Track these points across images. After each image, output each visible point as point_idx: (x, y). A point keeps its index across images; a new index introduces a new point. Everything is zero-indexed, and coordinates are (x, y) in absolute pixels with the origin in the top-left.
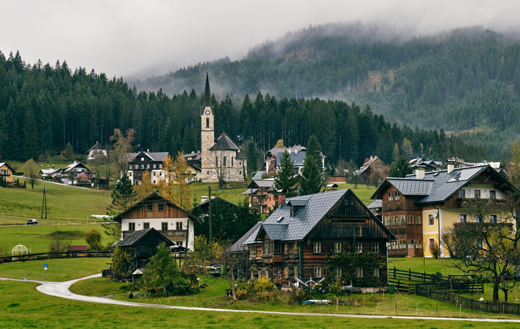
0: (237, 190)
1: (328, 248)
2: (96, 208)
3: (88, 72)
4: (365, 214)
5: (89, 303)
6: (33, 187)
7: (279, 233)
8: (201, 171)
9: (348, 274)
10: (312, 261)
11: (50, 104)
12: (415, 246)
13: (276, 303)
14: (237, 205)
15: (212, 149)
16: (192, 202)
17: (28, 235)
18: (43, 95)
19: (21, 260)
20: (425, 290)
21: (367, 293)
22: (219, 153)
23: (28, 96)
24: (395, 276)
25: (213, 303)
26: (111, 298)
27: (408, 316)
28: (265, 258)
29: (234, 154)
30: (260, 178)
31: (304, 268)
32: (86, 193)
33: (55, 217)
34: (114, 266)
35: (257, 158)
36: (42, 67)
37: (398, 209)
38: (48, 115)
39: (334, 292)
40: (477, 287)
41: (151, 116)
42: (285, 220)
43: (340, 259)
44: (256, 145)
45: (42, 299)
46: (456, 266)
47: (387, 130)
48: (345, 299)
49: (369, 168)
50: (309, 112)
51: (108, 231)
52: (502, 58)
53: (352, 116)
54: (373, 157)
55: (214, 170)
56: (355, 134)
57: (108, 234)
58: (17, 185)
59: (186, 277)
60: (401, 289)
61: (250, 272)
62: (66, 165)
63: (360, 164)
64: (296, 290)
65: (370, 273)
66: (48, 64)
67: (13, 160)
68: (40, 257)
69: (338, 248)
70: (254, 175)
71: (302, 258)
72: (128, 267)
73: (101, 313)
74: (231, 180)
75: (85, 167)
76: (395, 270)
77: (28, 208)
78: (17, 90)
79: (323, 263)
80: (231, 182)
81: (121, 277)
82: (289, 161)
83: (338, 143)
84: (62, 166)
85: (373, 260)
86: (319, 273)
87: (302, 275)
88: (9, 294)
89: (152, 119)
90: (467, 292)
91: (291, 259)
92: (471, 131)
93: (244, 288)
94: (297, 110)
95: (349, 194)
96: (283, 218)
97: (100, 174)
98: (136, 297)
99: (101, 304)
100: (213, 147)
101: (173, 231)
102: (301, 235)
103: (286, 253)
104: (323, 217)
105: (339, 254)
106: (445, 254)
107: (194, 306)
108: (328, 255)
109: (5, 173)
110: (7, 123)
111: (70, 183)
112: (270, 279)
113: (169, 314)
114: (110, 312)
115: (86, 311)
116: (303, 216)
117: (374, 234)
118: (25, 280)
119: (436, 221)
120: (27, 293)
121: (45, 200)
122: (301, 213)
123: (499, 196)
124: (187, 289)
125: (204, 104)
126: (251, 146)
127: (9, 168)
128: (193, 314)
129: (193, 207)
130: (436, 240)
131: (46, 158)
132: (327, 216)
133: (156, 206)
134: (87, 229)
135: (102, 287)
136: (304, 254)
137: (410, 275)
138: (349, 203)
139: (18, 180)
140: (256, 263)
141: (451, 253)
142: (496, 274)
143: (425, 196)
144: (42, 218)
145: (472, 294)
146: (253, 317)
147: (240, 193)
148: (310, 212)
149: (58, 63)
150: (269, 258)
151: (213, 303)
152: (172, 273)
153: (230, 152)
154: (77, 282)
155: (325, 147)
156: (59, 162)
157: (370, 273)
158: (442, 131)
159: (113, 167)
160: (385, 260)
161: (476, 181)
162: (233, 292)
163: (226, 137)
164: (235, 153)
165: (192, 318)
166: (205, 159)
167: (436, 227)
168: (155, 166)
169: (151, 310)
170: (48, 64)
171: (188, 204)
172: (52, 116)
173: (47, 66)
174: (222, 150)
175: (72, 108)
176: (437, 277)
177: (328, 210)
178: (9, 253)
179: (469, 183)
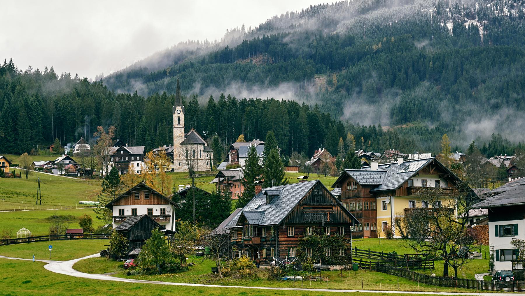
0: (205, 179)
1: (300, 232)
2: (83, 195)
3: (73, 77)
4: (332, 202)
5: (93, 280)
6: (27, 177)
7: (257, 218)
8: (173, 162)
9: (318, 254)
10: (287, 243)
11: (40, 104)
12: (370, 229)
13: (256, 279)
14: (211, 193)
15: (182, 144)
16: (171, 190)
17: (28, 219)
18: (34, 97)
19: (26, 242)
20: (384, 267)
21: (334, 270)
22: (189, 147)
23: (21, 98)
24: (356, 255)
25: (202, 279)
26: (111, 275)
27: (373, 290)
28: (246, 240)
29: (201, 148)
30: (225, 168)
31: (280, 249)
32: (74, 181)
33: (48, 203)
34: (112, 247)
35: (221, 151)
36: (32, 73)
37: (356, 197)
38: (38, 114)
39: (306, 269)
40: (429, 264)
41: (128, 115)
42: (261, 208)
43: (311, 241)
44: (220, 139)
45: (51, 277)
46: (412, 247)
47: (333, 126)
48: (317, 275)
49: (319, 159)
50: (265, 111)
51: (99, 216)
52: (431, 62)
53: (302, 114)
54: (322, 150)
55: (185, 162)
56: (306, 131)
57: (99, 218)
58: (14, 175)
59: (176, 256)
60: (365, 267)
61: (231, 252)
62: (55, 157)
63: (310, 156)
64: (273, 268)
65: (336, 253)
66: (38, 70)
67: (8, 153)
68: (41, 239)
69: (309, 232)
70: (219, 165)
71: (278, 240)
72: (124, 248)
73: (105, 289)
74: (199, 170)
75: (72, 160)
76: (356, 249)
77: (24, 195)
78: (11, 93)
79: (296, 244)
80: (200, 172)
81: (116, 254)
82: (256, 154)
83: (291, 138)
84: (52, 159)
85: (339, 242)
86: (292, 254)
87: (278, 255)
88: (21, 272)
89: (129, 117)
90: (420, 268)
91: (268, 241)
92: (404, 126)
93: (228, 267)
94: (255, 109)
95: (319, 185)
96: (260, 206)
97: (86, 165)
98: (134, 274)
99: (103, 281)
100: (183, 142)
101: (158, 216)
102: (277, 220)
103: (263, 236)
104: (296, 205)
105: (310, 236)
106: (397, 235)
107: (185, 282)
108: (300, 237)
109: (3, 165)
110: (3, 121)
111: (59, 173)
112: (249, 258)
113: (165, 289)
114: (112, 287)
115: (91, 287)
116: (278, 203)
117: (340, 219)
118: (33, 260)
119: (388, 207)
120: (37, 271)
121: (39, 189)
122: (276, 201)
123: (442, 184)
124: (178, 268)
125: (175, 104)
126: (216, 140)
127: (7, 160)
128: (186, 289)
129: (172, 195)
130: (389, 222)
131: (37, 151)
132: (299, 204)
133: (142, 195)
134: (80, 213)
135: (102, 266)
136: (280, 236)
137: (369, 254)
138: (318, 193)
139: (14, 171)
140: (237, 245)
141: (402, 233)
142: (446, 252)
143: (379, 185)
144: (37, 204)
145: (424, 270)
146: (238, 292)
147: (207, 181)
148: (284, 200)
149: (46, 68)
150: (249, 240)
151: (202, 279)
152: (164, 254)
153: (199, 145)
154: (79, 261)
155: (280, 140)
156: (49, 155)
157: (336, 253)
158: (380, 126)
159: (96, 159)
160: (349, 242)
161: (424, 171)
162: (219, 270)
163: (195, 132)
164: (203, 146)
165: (185, 293)
166: (177, 152)
167: (392, 212)
168: (133, 158)
169: (149, 286)
170: (38, 70)
171: (168, 192)
172: (42, 115)
173: (37, 72)
174: (192, 144)
175: (60, 108)
176: (392, 257)
177: (300, 198)
178: (14, 235)
179: (417, 174)
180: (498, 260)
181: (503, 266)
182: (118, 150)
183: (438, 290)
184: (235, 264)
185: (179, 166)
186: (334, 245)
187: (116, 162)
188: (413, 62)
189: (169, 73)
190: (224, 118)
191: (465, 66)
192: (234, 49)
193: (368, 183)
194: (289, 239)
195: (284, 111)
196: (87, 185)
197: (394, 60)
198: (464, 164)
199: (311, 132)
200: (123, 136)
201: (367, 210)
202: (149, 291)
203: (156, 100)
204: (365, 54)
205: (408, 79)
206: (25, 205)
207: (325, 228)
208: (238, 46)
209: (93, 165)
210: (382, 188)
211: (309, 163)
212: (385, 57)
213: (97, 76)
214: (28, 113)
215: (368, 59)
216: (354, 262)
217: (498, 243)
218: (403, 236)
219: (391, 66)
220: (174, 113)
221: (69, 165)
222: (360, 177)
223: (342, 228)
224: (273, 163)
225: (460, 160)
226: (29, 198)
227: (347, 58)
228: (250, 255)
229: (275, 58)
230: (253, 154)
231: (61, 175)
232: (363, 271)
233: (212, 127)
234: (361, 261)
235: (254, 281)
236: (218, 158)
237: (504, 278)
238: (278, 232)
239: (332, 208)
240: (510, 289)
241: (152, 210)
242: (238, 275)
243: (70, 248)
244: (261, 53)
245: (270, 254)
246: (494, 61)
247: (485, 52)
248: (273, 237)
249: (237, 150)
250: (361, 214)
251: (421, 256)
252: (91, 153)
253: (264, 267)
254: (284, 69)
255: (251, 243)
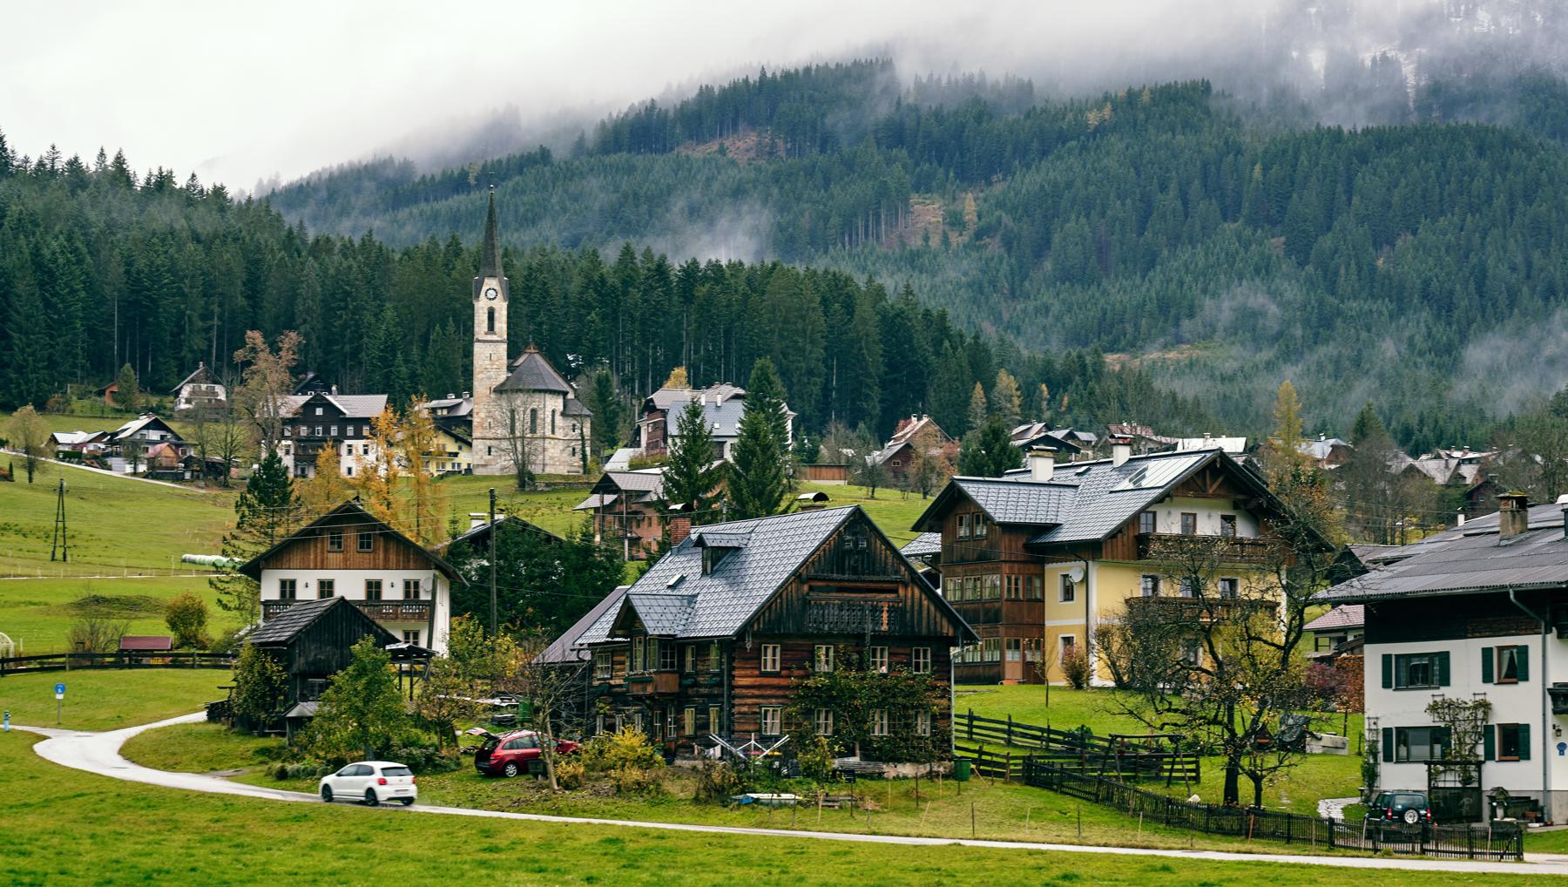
0: (564, 496)
1: (799, 656)
2: (195, 535)
4: (897, 572)
5: (172, 790)
6: (30, 480)
8: (470, 445)
10: (757, 692)
11: (80, 262)
12: (1024, 656)
15: (500, 390)
16: (446, 526)
17: (17, 604)
20: (1048, 771)
21: (897, 778)
22: (519, 400)
23: (22, 241)
24: (970, 733)
26: (229, 778)
30: (626, 467)
32: (171, 495)
33: (88, 559)
35: (616, 414)
36: (58, 166)
38: (73, 292)
39: (812, 773)
40: (1184, 766)
41: (344, 300)
42: (687, 585)
43: (831, 688)
44: (615, 380)
45: (48, 778)
47: (955, 349)
48: (841, 792)
49: (908, 446)
50: (755, 297)
51: (225, 599)
52: (1258, 167)
53: (864, 309)
54: (919, 419)
56: (875, 359)
57: (225, 607)
59: (427, 726)
60: (991, 770)
61: (594, 717)
63: (884, 433)
66: (76, 159)
68: (45, 664)
70: (609, 457)
72: (274, 698)
73: (202, 819)
74: (548, 470)
77: (17, 532)
79: (785, 697)
80: (549, 475)
83: (828, 381)
84: (108, 426)
86: (773, 725)
89: (345, 308)
90: (1158, 778)
91: (701, 686)
95: (858, 520)
96: (682, 579)
97: (208, 448)
98: (296, 775)
99: (202, 794)
103: (689, 669)
106: (1101, 676)
107: (446, 804)
111: (129, 469)
112: (644, 737)
114: (224, 815)
116: (734, 573)
117: (920, 623)
119: (1079, 593)
120: (10, 760)
121: (61, 516)
123: (1244, 530)
126: (603, 383)
129: (448, 542)
131: (68, 402)
132: (797, 576)
133: (351, 537)
134: (171, 590)
135: (206, 749)
137: (1010, 732)
138: (856, 544)
140: (610, 694)
143: (1055, 527)
146: (599, 838)
147: (571, 504)
150: (644, 681)
152: (388, 717)
153: (548, 396)
155: (796, 388)
160: (946, 693)
163: (538, 357)
166: (482, 415)
168: (350, 430)
170: (76, 159)
172: (83, 294)
173: (74, 164)
174: (528, 391)
176: (1078, 741)
177: (801, 560)
179: (1168, 495)
180: (1388, 758)
181: (1405, 779)
182: (306, 405)
183: (1199, 843)
184: (601, 752)
185: (486, 456)
186: (901, 703)
187: (299, 440)
188: (1205, 165)
189: (477, 179)
190: (631, 316)
191: (1358, 181)
192: (671, 114)
193: (1020, 518)
194: (766, 681)
195: (811, 301)
196: (212, 508)
197: (1147, 156)
198: (1339, 474)
199: (888, 365)
200: (326, 362)
201: (1017, 600)
202: (332, 828)
203: (429, 258)
204: (1063, 138)
205: (1186, 216)
206: (19, 561)
207: (874, 651)
208: (684, 104)
209: (231, 448)
210: (1063, 536)
211: (877, 457)
212: (1121, 146)
213: (261, 181)
214: (41, 285)
215: (1070, 152)
216: (958, 753)
217: (1392, 708)
218: (1119, 680)
219: (1138, 174)
220: (478, 296)
221: (158, 447)
222: (999, 500)
223: (925, 652)
224: (754, 454)
225: (1330, 462)
226: (31, 542)
227: (1009, 147)
228: (649, 729)
229: (793, 141)
230: (693, 423)
231: (135, 474)
232: (982, 782)
233: (594, 343)
234: (981, 752)
235: (653, 805)
236: (607, 435)
237: (1401, 814)
238: (731, 659)
239: (896, 591)
240: (1409, 847)
241: (378, 584)
242: (607, 785)
243: (125, 692)
244: (753, 124)
245: (706, 726)
246: (1444, 165)
247: (1418, 140)
248: (715, 675)
249: (664, 413)
250: (998, 612)
251: (1165, 742)
252: (224, 413)
253: (686, 764)
254: (819, 175)
255: (650, 690)
